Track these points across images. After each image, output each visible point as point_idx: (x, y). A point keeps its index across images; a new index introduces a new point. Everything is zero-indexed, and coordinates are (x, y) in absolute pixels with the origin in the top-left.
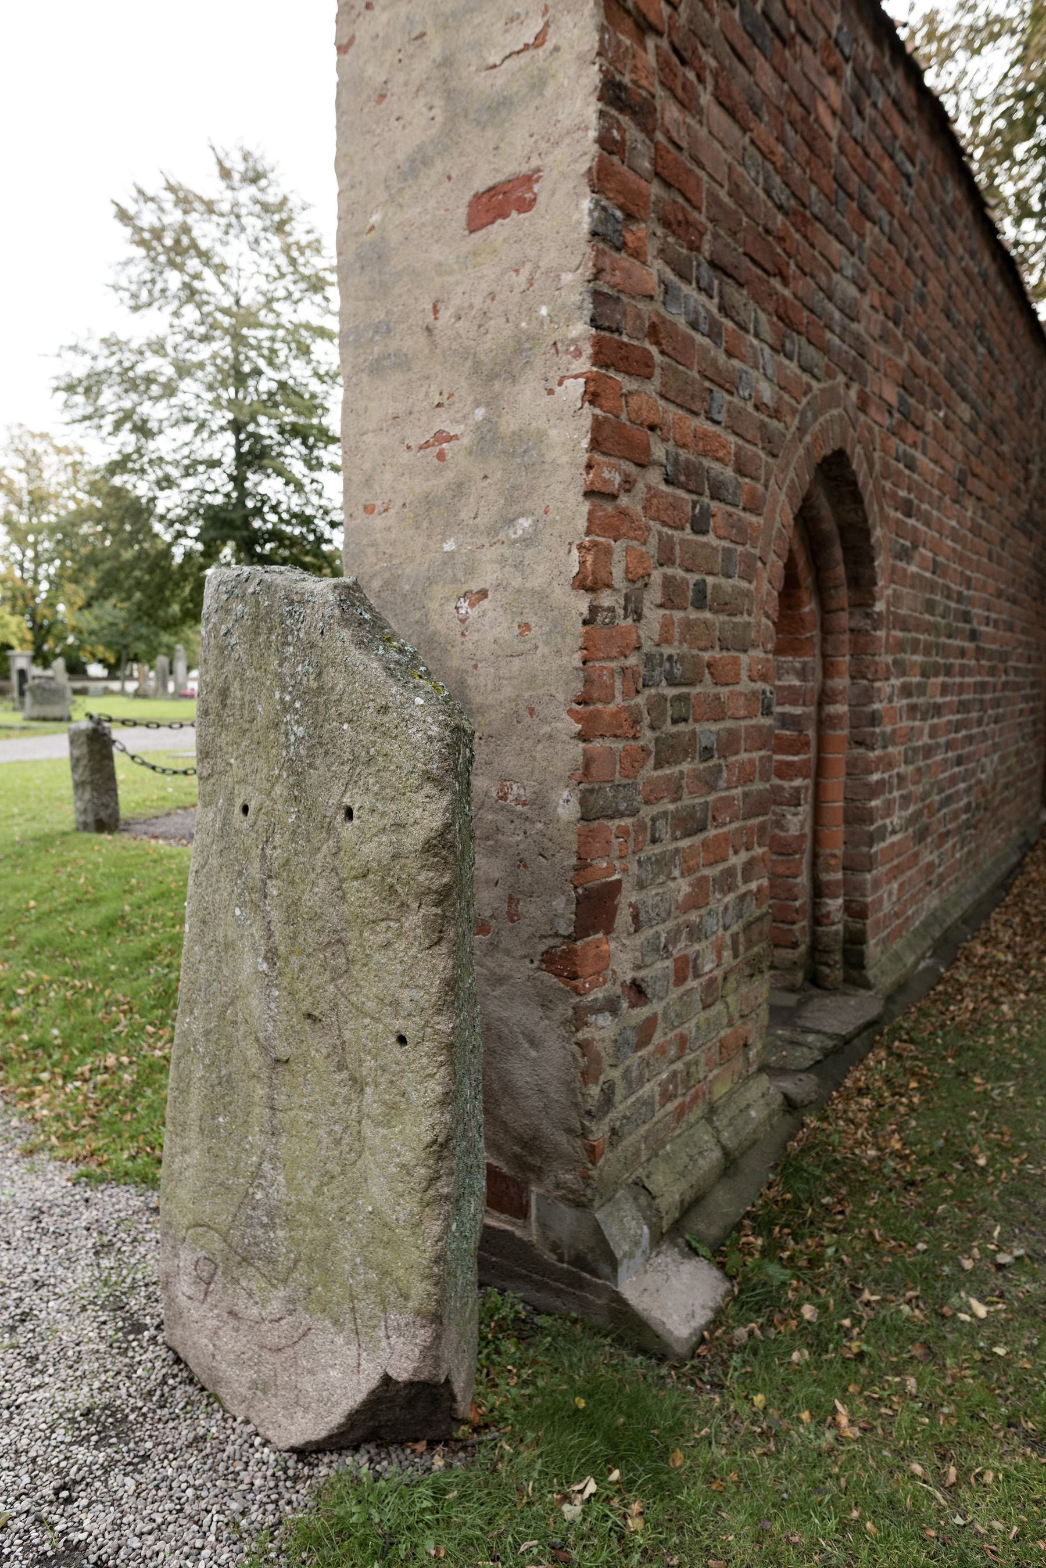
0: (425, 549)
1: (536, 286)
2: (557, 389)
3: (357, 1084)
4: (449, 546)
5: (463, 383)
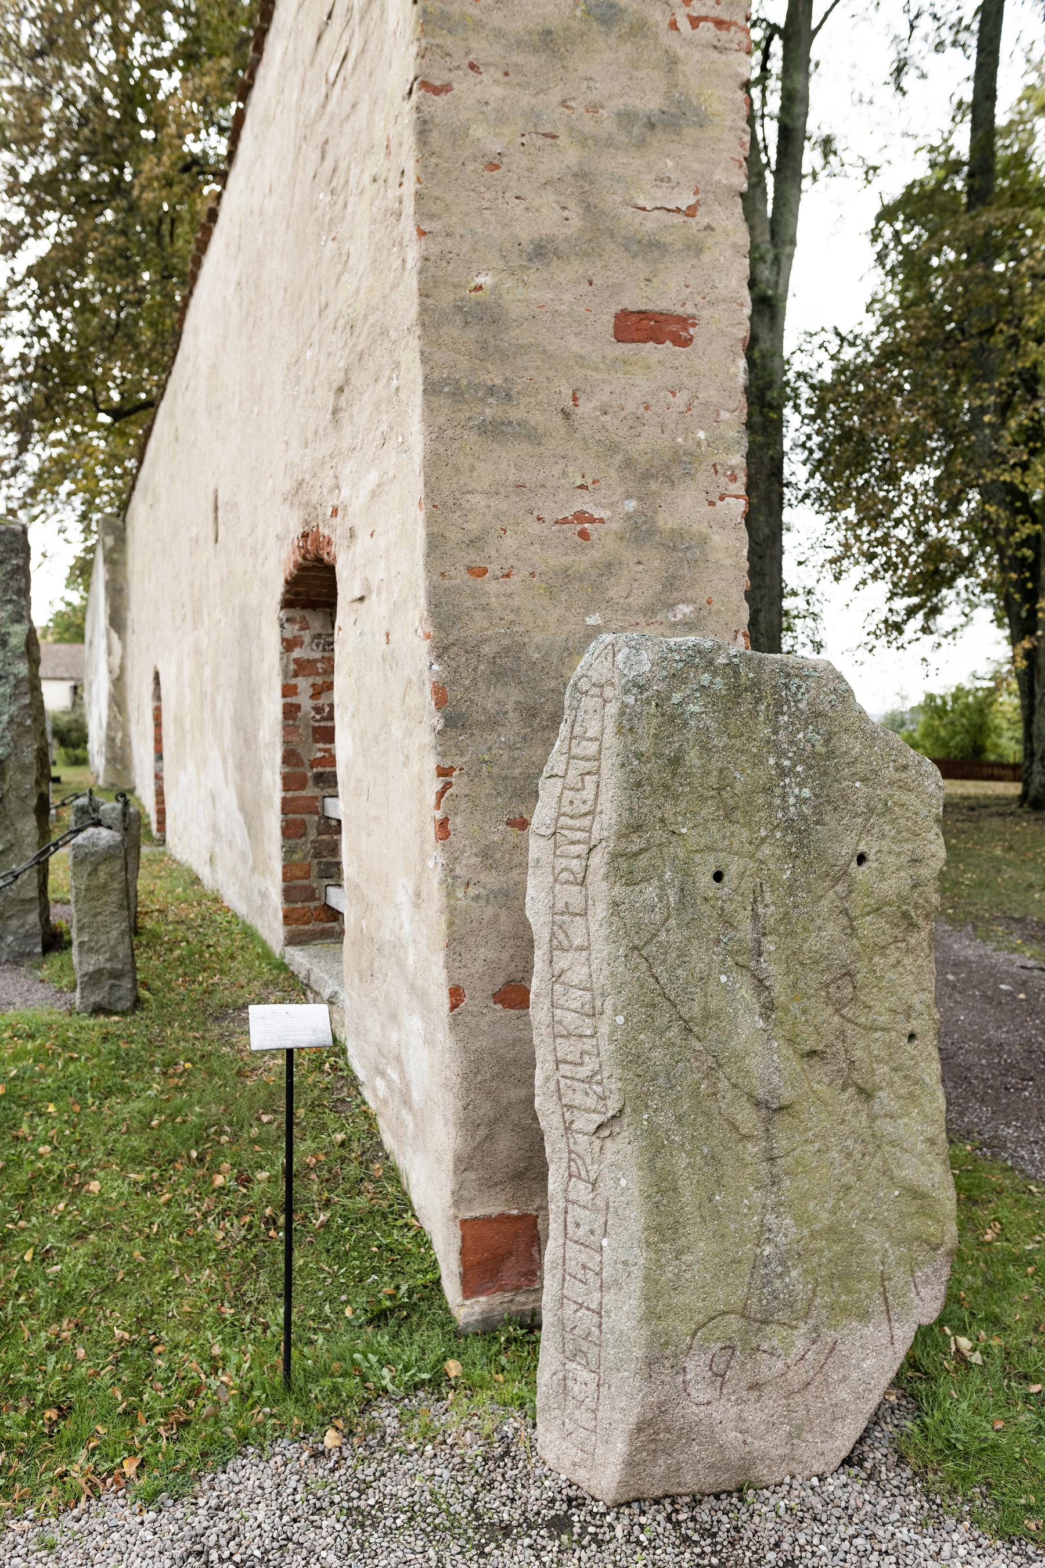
0: (561, 621)
1: (694, 411)
2: (719, 503)
3: (866, 1094)
5: (613, 473)
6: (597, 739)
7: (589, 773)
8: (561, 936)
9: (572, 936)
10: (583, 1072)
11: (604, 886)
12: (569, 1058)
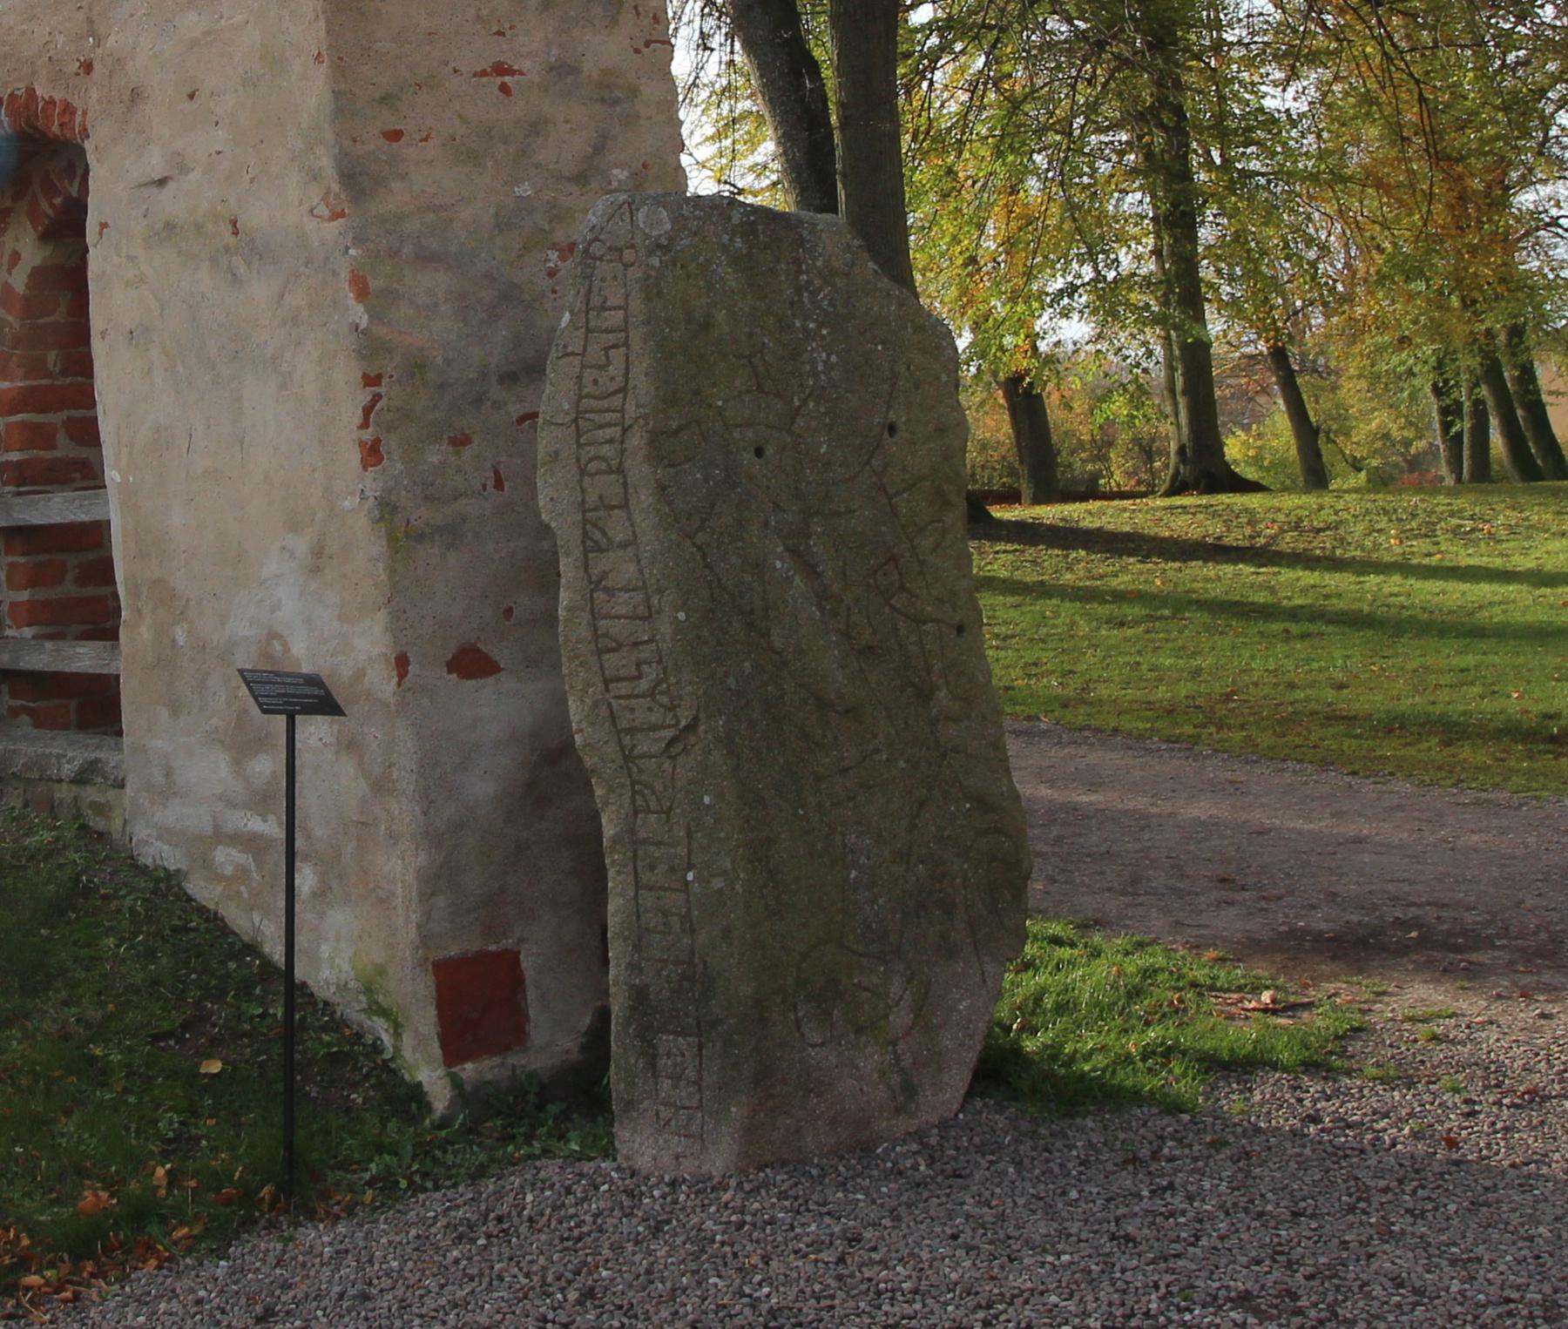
2: (645, 50)
4: (525, 190)
6: (620, 308)
7: (615, 346)
8: (597, 535)
9: (611, 533)
10: (644, 685)
11: (646, 469)
12: (622, 673)
